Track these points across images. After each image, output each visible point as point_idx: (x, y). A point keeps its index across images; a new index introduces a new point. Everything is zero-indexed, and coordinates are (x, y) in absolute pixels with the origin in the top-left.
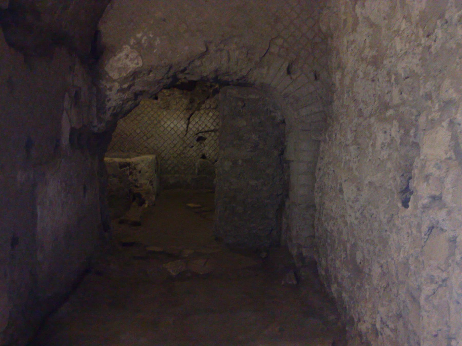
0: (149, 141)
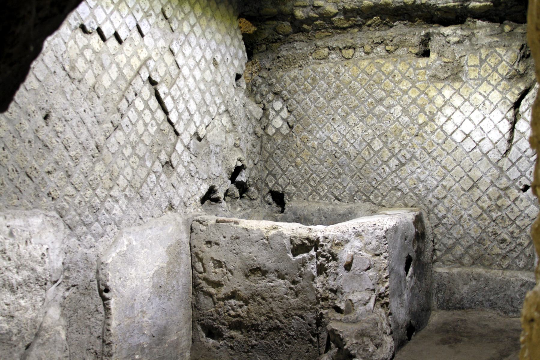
0: (407, 168)
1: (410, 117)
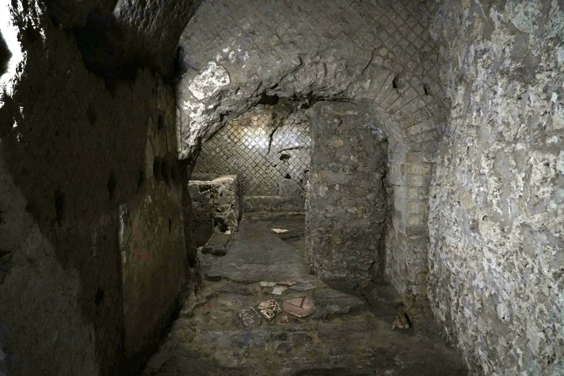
1: (231, 139)
